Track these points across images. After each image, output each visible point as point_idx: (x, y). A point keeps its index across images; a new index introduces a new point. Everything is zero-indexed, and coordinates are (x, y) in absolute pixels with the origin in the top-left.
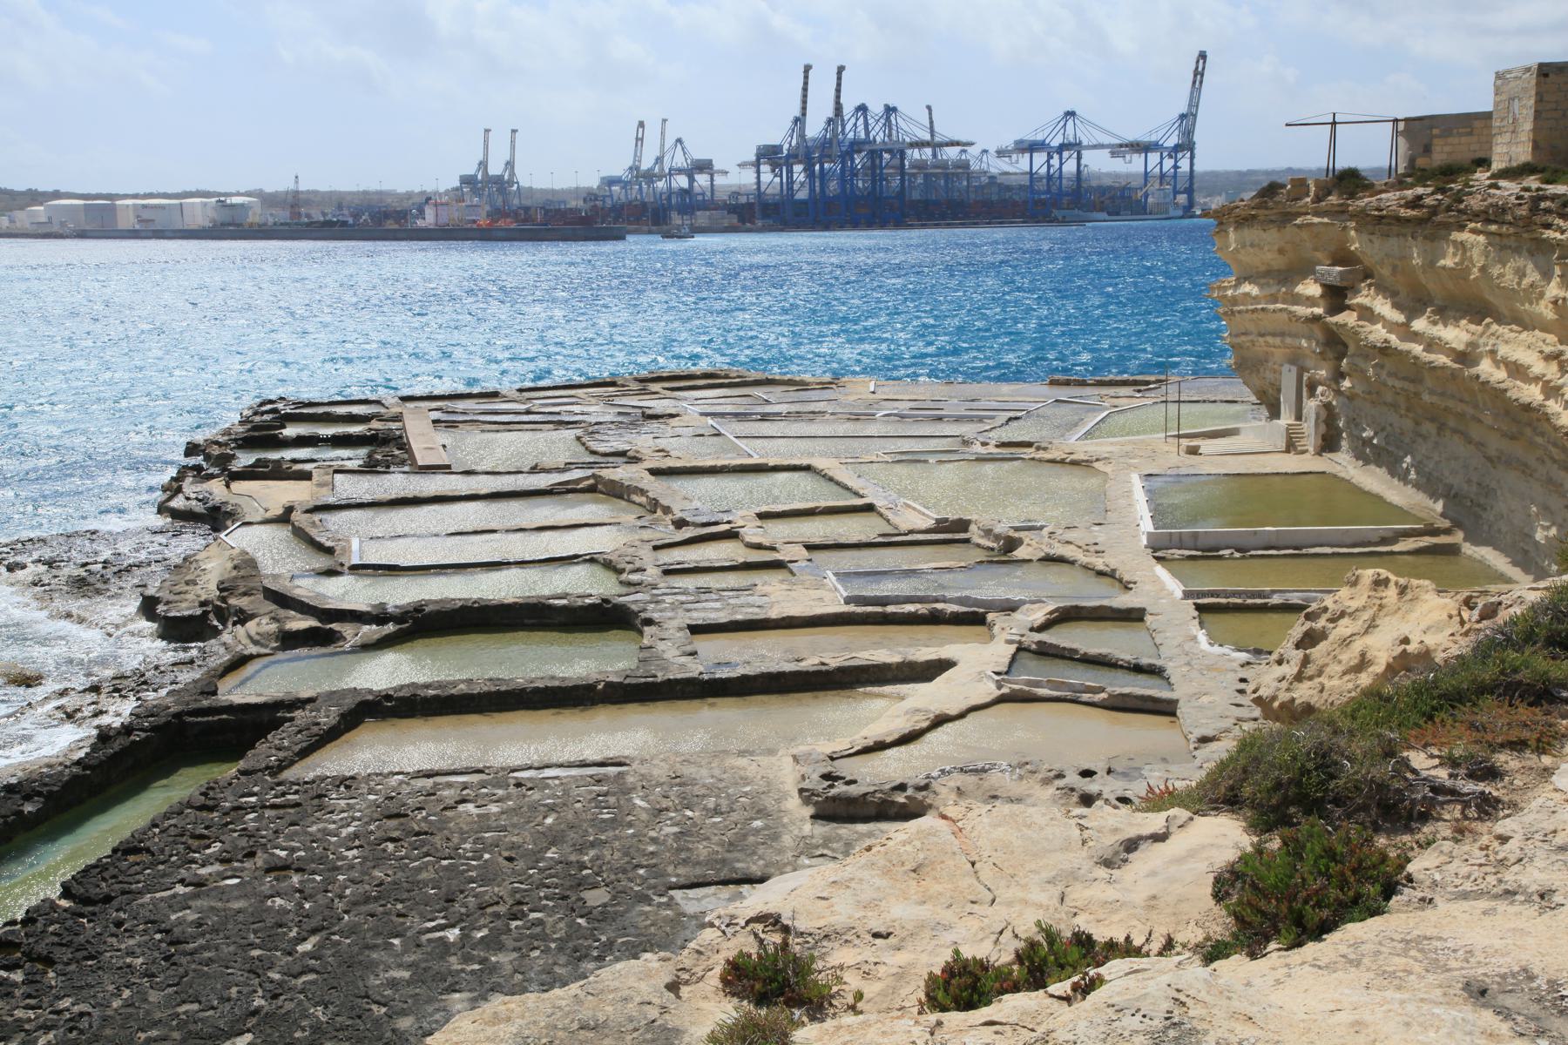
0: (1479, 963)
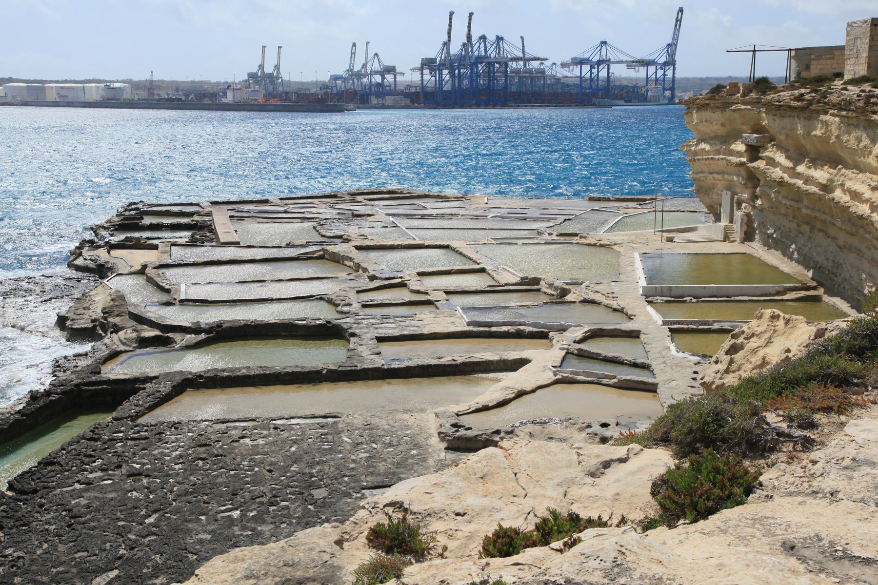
0: (793, 531)
